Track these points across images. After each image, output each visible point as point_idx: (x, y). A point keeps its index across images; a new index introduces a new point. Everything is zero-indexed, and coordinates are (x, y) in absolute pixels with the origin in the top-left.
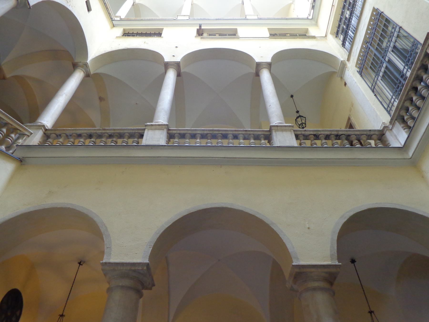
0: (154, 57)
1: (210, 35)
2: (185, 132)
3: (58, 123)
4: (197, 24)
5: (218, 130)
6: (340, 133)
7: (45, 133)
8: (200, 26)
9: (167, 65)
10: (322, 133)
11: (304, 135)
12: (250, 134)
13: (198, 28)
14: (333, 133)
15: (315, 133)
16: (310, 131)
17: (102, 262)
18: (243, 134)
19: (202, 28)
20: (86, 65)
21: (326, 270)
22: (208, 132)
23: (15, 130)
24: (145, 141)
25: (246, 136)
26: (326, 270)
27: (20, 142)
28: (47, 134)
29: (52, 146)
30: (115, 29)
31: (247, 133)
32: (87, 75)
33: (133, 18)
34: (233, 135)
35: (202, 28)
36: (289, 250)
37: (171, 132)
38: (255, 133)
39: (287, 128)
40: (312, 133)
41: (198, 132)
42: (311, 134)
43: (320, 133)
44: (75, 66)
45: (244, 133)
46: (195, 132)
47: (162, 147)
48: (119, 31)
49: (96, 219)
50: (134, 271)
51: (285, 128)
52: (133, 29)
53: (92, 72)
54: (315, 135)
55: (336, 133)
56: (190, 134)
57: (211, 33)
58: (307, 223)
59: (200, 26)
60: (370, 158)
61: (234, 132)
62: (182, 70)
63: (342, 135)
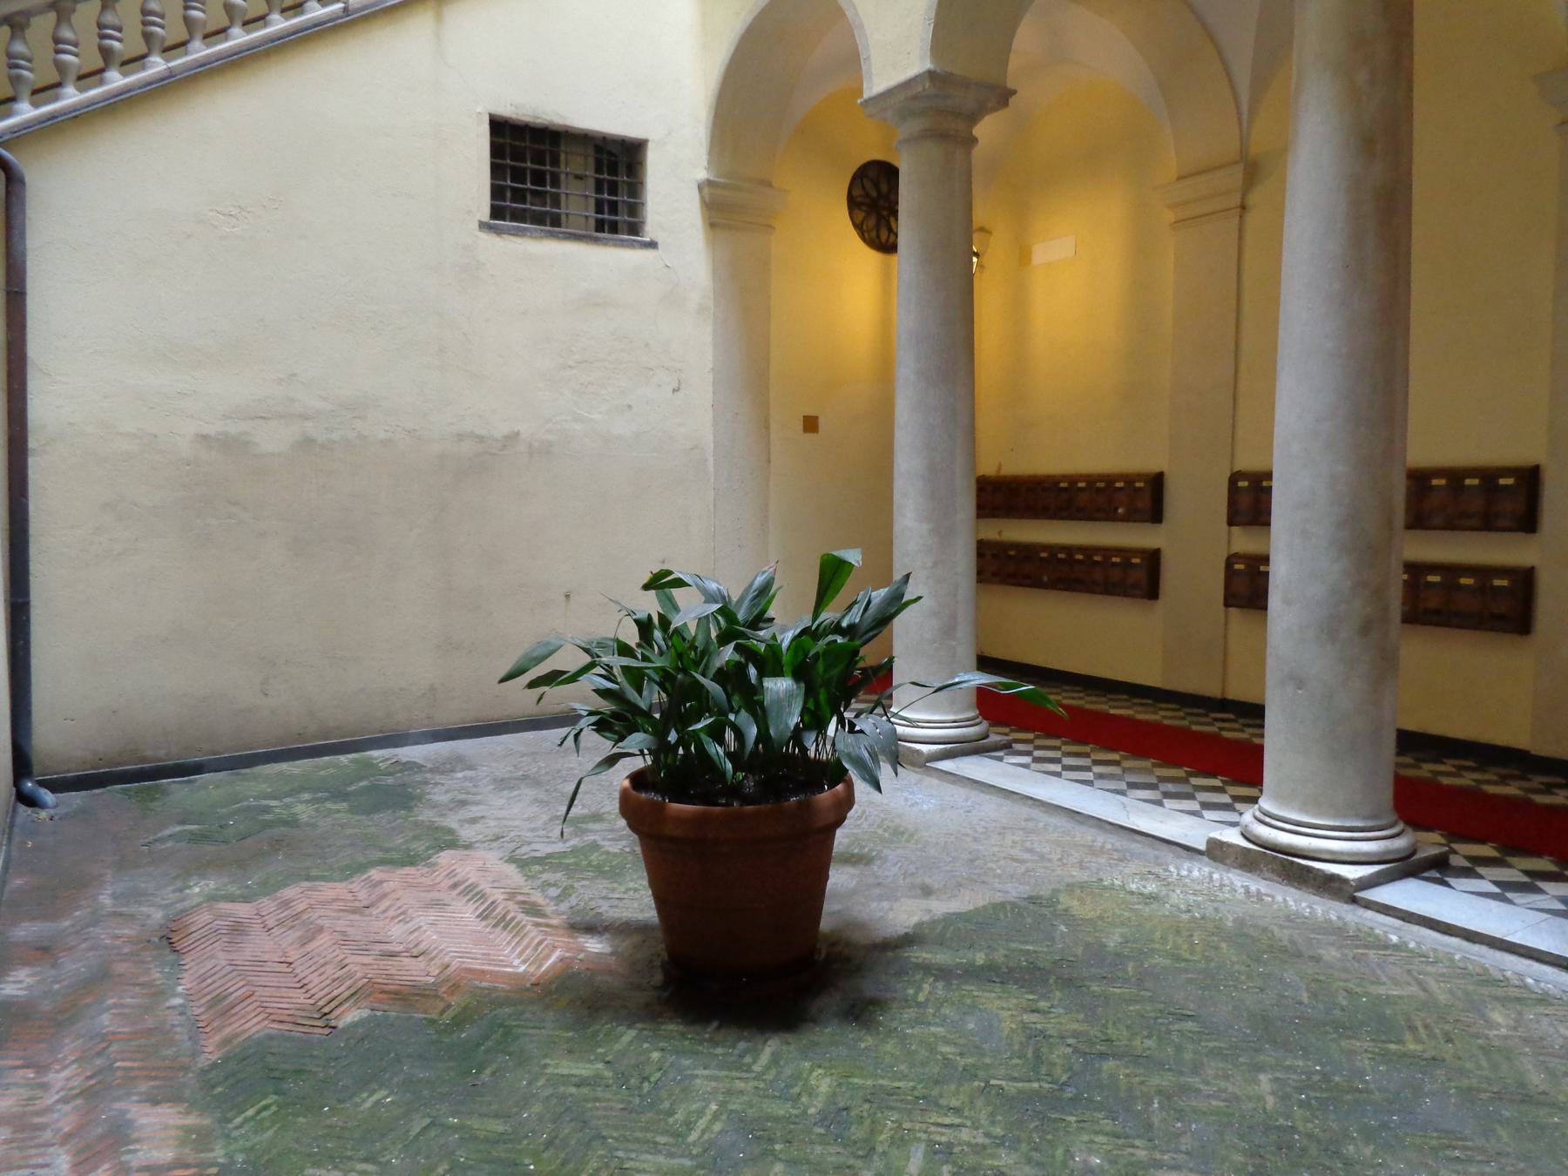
50: (914, 98)
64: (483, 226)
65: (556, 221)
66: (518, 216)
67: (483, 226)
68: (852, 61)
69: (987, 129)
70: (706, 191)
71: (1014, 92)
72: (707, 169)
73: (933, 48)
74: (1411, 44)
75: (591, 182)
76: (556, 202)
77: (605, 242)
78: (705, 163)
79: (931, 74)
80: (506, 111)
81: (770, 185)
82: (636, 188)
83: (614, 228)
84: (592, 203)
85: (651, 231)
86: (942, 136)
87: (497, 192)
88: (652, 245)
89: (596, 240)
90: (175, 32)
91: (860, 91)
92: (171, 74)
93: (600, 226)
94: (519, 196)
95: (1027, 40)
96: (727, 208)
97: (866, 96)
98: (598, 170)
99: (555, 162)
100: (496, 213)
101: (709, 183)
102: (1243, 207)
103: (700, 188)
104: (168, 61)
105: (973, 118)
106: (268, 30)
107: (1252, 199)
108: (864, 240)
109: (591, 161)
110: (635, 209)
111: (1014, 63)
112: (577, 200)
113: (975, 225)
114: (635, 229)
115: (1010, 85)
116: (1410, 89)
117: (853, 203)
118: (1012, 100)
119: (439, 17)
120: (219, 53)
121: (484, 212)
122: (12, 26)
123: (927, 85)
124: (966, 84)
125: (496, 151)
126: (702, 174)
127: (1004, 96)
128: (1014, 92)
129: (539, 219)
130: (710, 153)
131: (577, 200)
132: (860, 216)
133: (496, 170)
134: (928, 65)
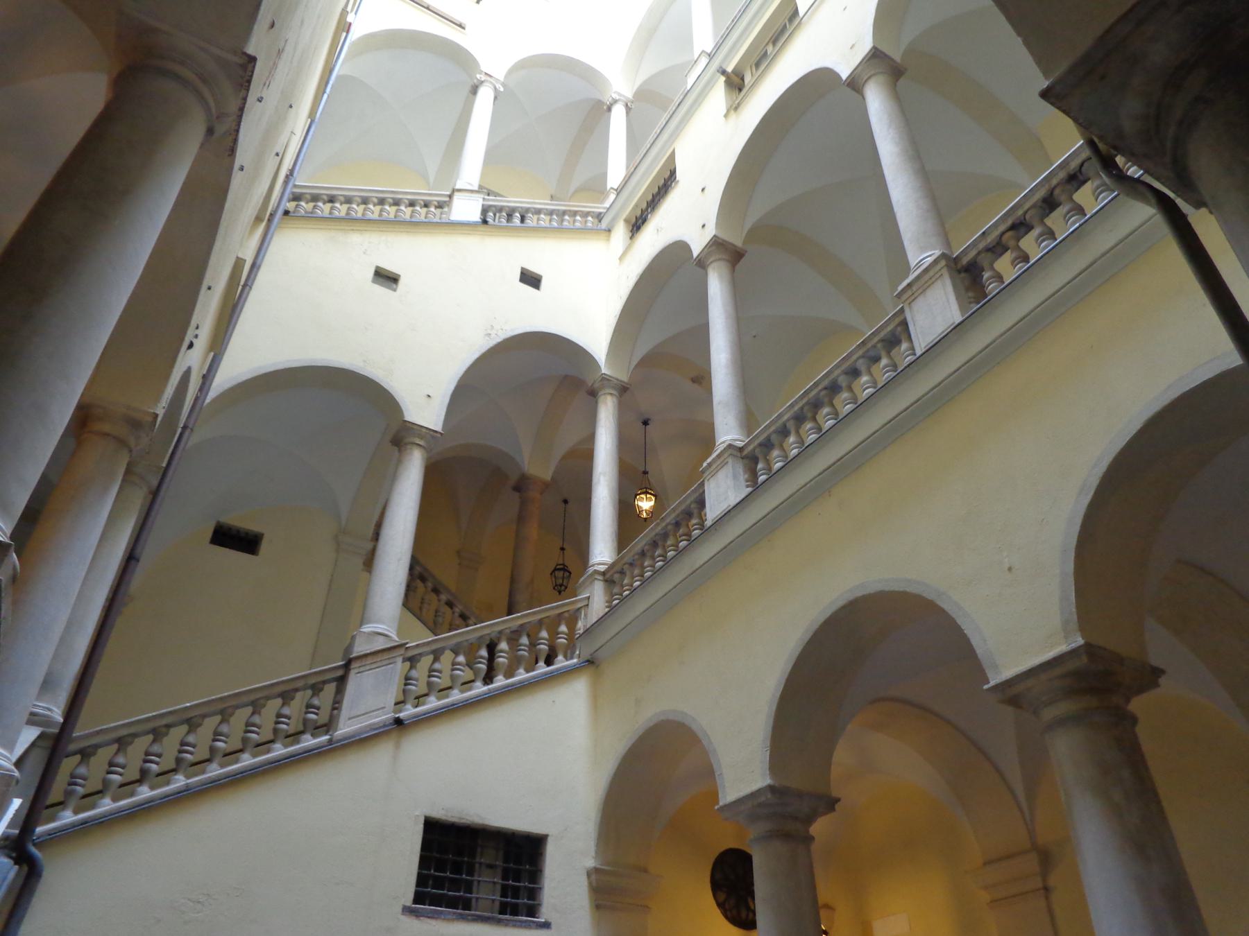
0: (816, 84)
1: (758, 65)
2: (765, 435)
3: (748, 420)
4: (713, 76)
5: (816, 385)
6: (1074, 165)
7: (606, 581)
8: (724, 72)
9: (855, 84)
10: (1027, 206)
11: (989, 250)
12: (874, 346)
13: (723, 79)
14: (1054, 182)
15: (1009, 222)
16: (995, 225)
17: (986, 687)
18: (863, 357)
19: (730, 69)
20: (605, 379)
21: (1058, 671)
22: (800, 404)
23: (559, 618)
24: (713, 511)
25: (872, 353)
26: (1058, 671)
27: (581, 626)
28: (750, 458)
29: (773, 476)
30: (613, 234)
31: (869, 345)
32: (623, 390)
33: (666, 116)
34: (846, 373)
35: (730, 69)
36: (978, 651)
37: (745, 452)
38: (882, 334)
39: (931, 273)
40: (1002, 228)
41: (786, 418)
42: (1003, 233)
43: (1020, 212)
44: (593, 394)
45: (860, 353)
46: (780, 422)
47: (727, 518)
48: (621, 231)
49: (694, 727)
50: (760, 805)
51: (927, 277)
52: (636, 205)
53: (624, 377)
54: (1013, 227)
55: (1062, 175)
56: (775, 432)
57: (755, 58)
58: (1005, 554)
59: (724, 72)
60: (1136, 223)
61: (844, 367)
62: (897, 56)
63: (1082, 165)
64: (407, 910)
65: (467, 905)
66: (436, 901)
67: (407, 910)
68: (708, 773)
69: (819, 828)
70: (593, 877)
71: (838, 800)
72: (595, 858)
73: (904, 594)
74: (1147, 768)
75: (499, 871)
76: (469, 887)
77: (506, 924)
78: (593, 854)
79: (771, 788)
80: (438, 813)
81: (646, 871)
82: (535, 874)
83: (515, 911)
84: (499, 887)
85: (545, 913)
86: (787, 836)
87: (421, 880)
88: (546, 925)
89: (499, 922)
90: (443, 681)
91: (714, 795)
92: (187, 788)
93: (503, 911)
94: (439, 883)
95: (842, 756)
96: (607, 891)
97: (721, 803)
98: (506, 860)
99: (472, 854)
100: (419, 898)
101: (596, 870)
102: (1046, 889)
103: (589, 874)
104: (188, 777)
105: (809, 820)
106: (133, 799)
107: (1052, 881)
108: (726, 917)
109: (501, 853)
110: (534, 893)
111: (835, 771)
112: (487, 888)
113: (821, 900)
114: (532, 911)
115: (835, 793)
116: (1159, 802)
117: (716, 886)
118: (837, 807)
119: (398, 746)
120: (229, 772)
121: (408, 898)
122: (283, 699)
123: (769, 796)
124: (800, 795)
125: (426, 845)
126: (590, 863)
127: (830, 804)
128: (838, 800)
129: (452, 903)
130: (597, 845)
131: (487, 888)
132: (722, 897)
133: (424, 862)
134: (768, 781)
